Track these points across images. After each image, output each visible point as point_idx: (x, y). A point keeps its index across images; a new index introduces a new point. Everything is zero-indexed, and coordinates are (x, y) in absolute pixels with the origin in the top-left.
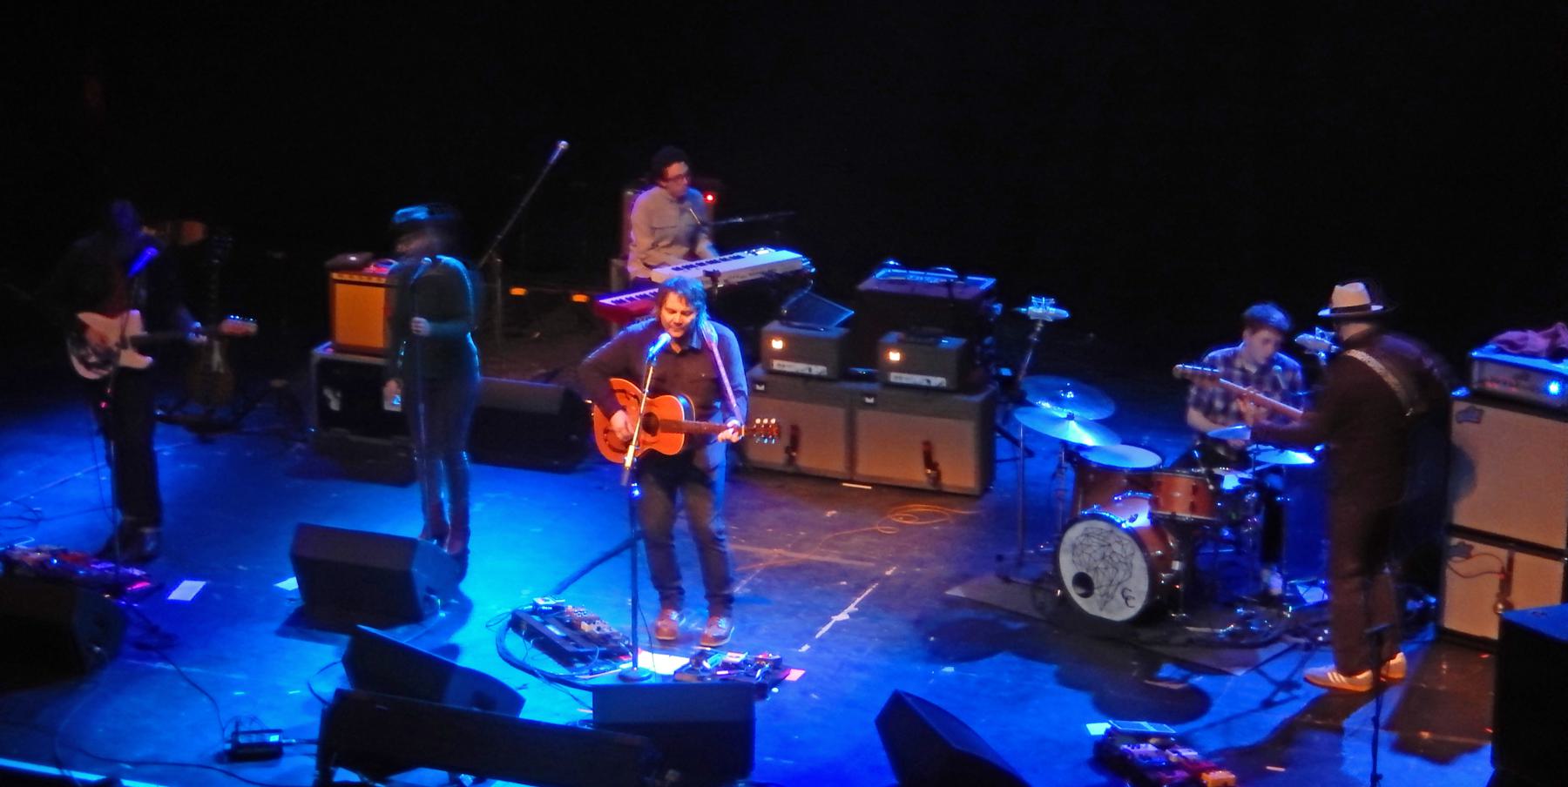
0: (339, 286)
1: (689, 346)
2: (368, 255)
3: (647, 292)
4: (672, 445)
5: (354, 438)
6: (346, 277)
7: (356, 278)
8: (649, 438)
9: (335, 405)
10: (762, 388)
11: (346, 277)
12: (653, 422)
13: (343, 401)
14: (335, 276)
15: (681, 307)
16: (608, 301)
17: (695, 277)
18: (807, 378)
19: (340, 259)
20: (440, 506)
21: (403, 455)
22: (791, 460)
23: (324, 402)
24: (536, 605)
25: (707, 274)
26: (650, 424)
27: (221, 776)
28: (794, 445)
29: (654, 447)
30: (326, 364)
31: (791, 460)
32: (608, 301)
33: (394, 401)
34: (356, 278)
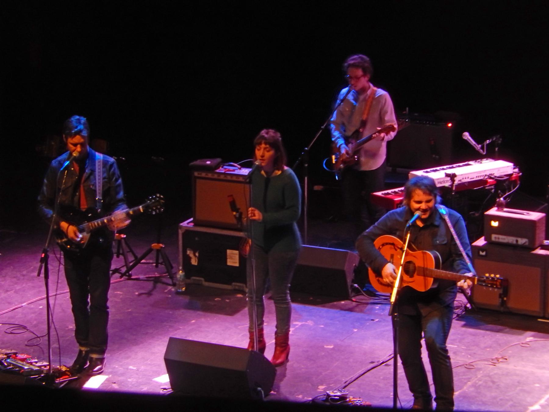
0: (198, 181)
1: (432, 219)
2: (219, 160)
3: (396, 190)
4: (420, 285)
5: (206, 284)
6: (203, 175)
7: (210, 175)
8: (406, 278)
9: (194, 262)
10: (484, 253)
11: (203, 175)
12: (411, 267)
13: (200, 259)
14: (196, 174)
15: (424, 198)
16: (379, 194)
17: (323, 374)
18: (515, 247)
19: (198, 162)
20: (431, 171)
21: (240, 296)
22: (503, 303)
23: (187, 259)
24: (328, 395)
25: (447, 175)
26: (408, 269)
27: (433, 173)
28: (505, 293)
29: (410, 285)
30: (188, 233)
31: (503, 303)
32: (379, 194)
33: (233, 259)
34: (210, 175)
